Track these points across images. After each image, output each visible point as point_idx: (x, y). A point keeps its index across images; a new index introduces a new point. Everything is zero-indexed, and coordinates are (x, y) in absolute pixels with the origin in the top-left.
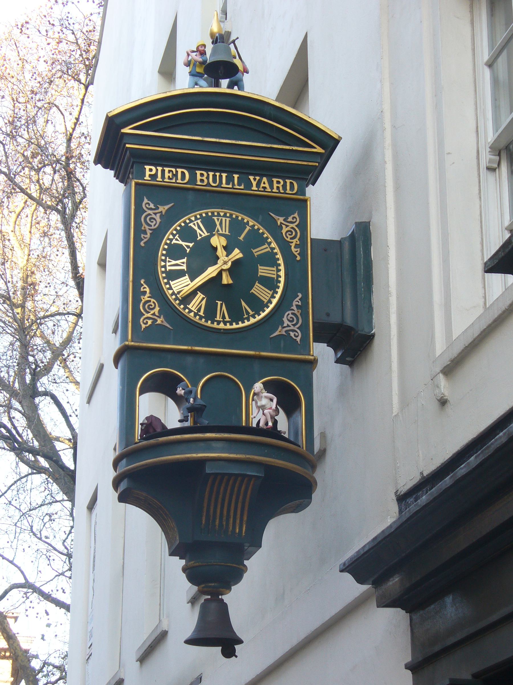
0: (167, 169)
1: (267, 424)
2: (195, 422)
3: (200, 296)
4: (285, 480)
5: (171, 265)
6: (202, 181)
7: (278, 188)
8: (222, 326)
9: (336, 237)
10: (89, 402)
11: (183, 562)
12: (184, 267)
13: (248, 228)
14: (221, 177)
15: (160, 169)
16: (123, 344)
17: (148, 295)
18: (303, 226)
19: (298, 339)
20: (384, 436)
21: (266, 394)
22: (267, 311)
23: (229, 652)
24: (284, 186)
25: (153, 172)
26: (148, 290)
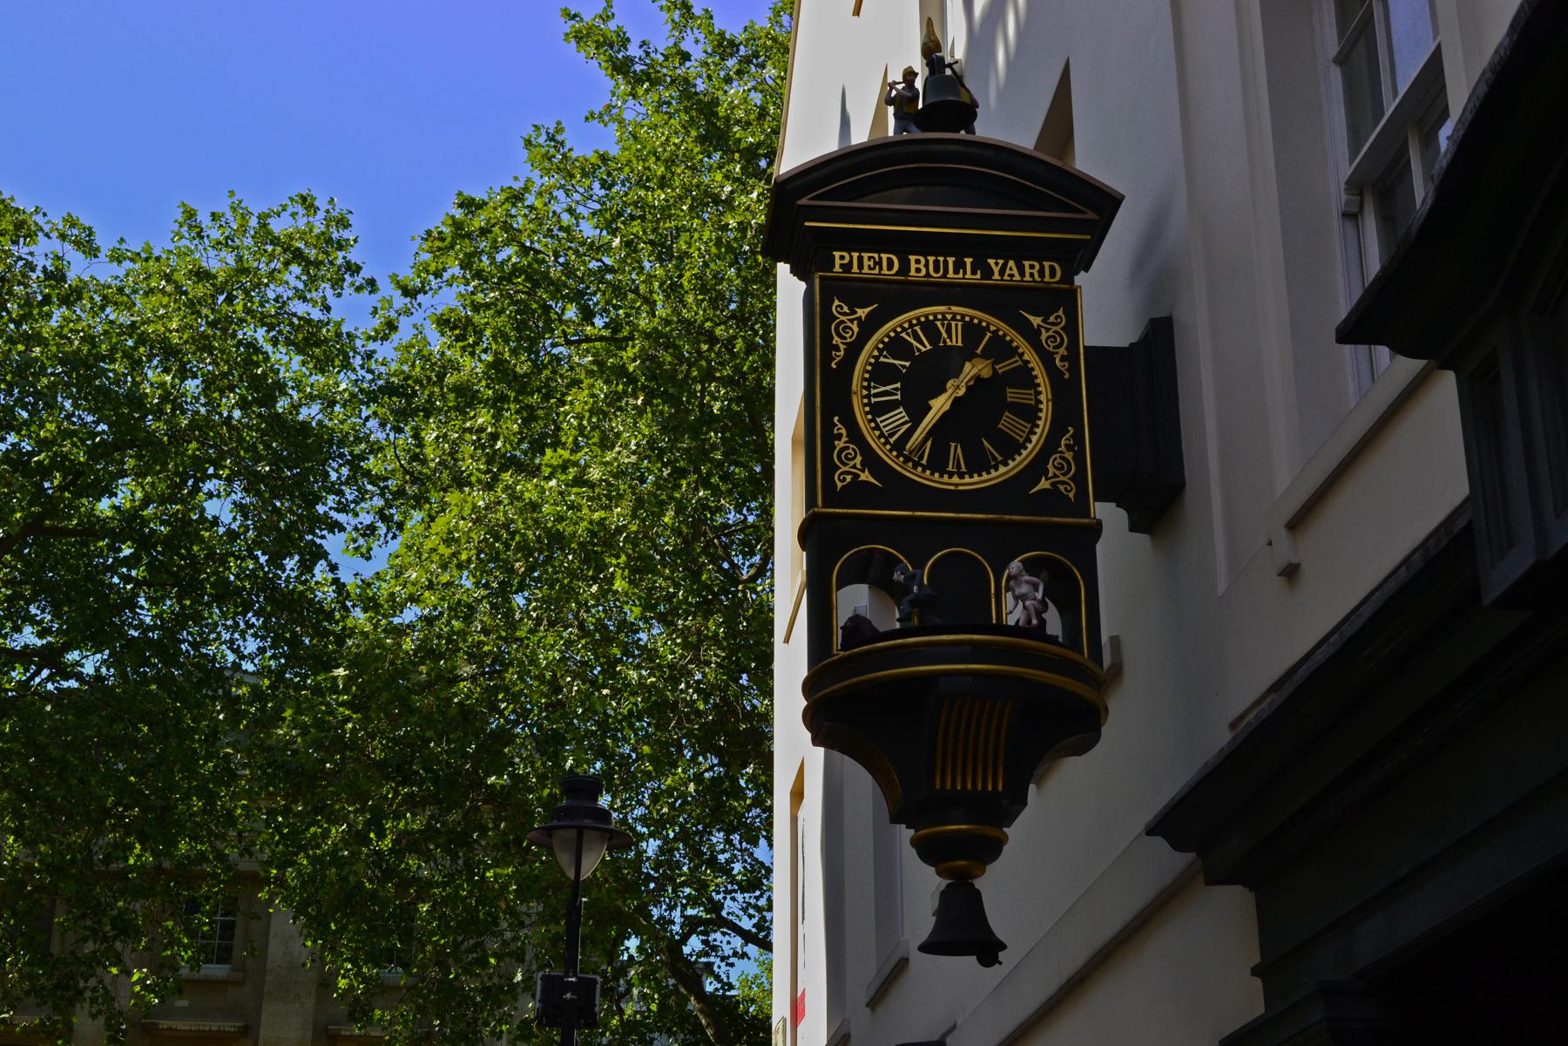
0: (866, 255)
1: (1029, 621)
2: (920, 621)
4: (1057, 709)
6: (918, 270)
7: (1032, 275)
10: (954, 1027)
11: (912, 832)
14: (946, 262)
15: (855, 255)
17: (844, 439)
18: (1072, 328)
19: (1071, 495)
24: (1041, 272)
25: (846, 261)
26: (843, 431)
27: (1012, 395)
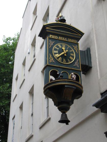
0: (54, 36)
3: (60, 58)
5: (55, 52)
8: (64, 63)
9: (84, 50)
10: (20, 88)
12: (57, 52)
13: (68, 47)
16: (46, 65)
18: (78, 48)
20: (93, 87)
21: (74, 75)
22: (73, 61)
23: (67, 124)
27: (71, 54)
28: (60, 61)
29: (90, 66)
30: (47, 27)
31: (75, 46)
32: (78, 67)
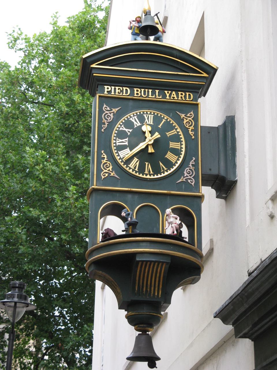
0: (117, 88)
3: (136, 159)
5: (119, 142)
8: (148, 177)
12: (127, 143)
18: (196, 119)
22: (175, 168)
27: (172, 145)
28: (134, 173)
29: (231, 178)
30: (92, 64)
31: (186, 113)
32: (193, 184)
